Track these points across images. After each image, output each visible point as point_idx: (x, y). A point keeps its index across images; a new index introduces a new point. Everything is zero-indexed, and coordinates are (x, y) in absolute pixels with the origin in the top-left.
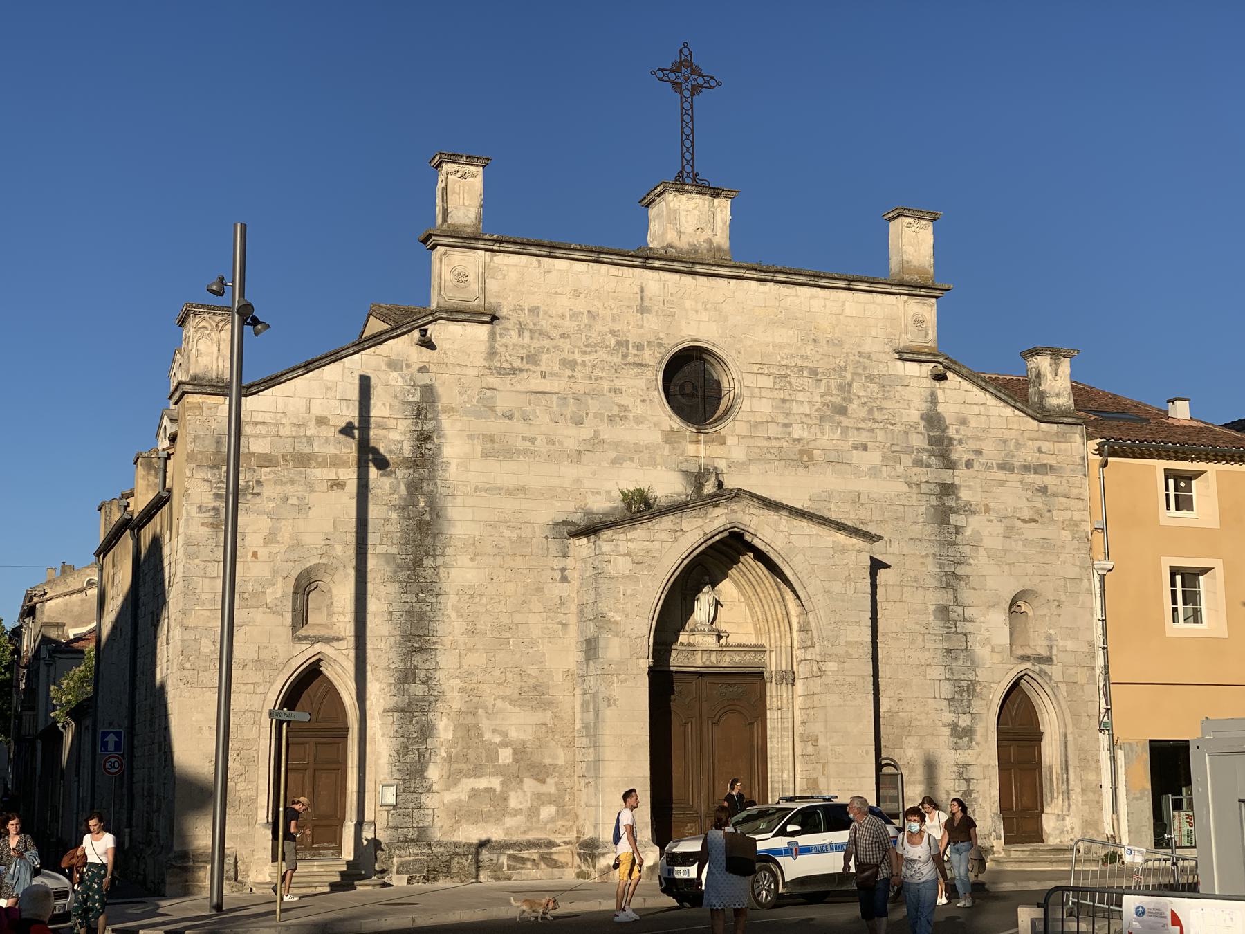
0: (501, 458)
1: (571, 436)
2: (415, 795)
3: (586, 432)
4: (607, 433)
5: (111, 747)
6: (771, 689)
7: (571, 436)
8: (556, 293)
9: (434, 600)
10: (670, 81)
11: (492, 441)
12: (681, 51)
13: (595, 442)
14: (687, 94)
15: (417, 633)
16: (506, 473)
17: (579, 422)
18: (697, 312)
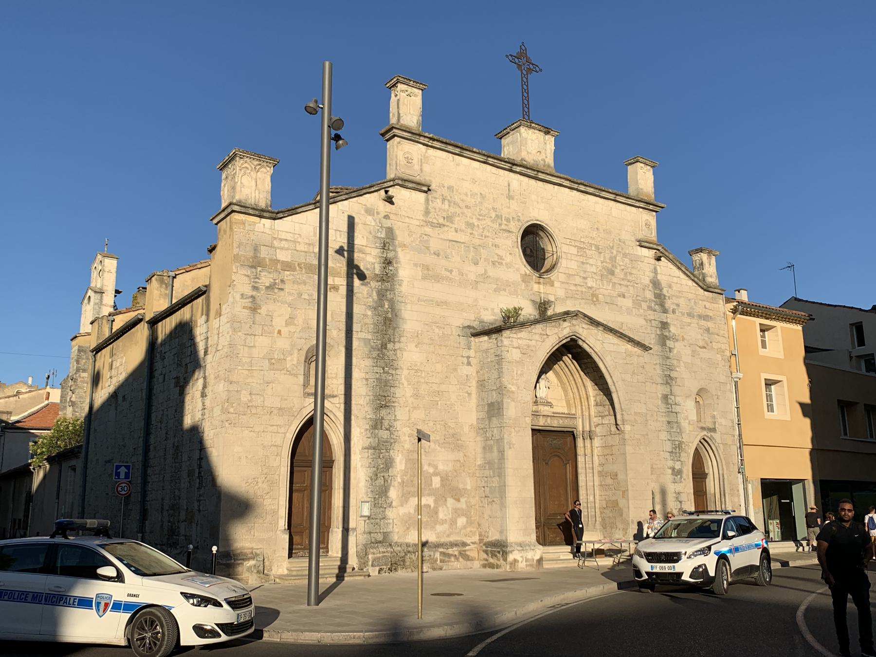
0: (433, 281)
1: (472, 272)
2: (382, 509)
3: (480, 270)
4: (492, 272)
5: (122, 476)
6: (580, 442)
7: (472, 272)
8: (463, 179)
9: (394, 372)
10: (533, 64)
11: (428, 269)
12: (521, 46)
13: (485, 277)
14: (524, 72)
15: (383, 394)
16: (436, 291)
17: (476, 264)
18: (538, 202)
